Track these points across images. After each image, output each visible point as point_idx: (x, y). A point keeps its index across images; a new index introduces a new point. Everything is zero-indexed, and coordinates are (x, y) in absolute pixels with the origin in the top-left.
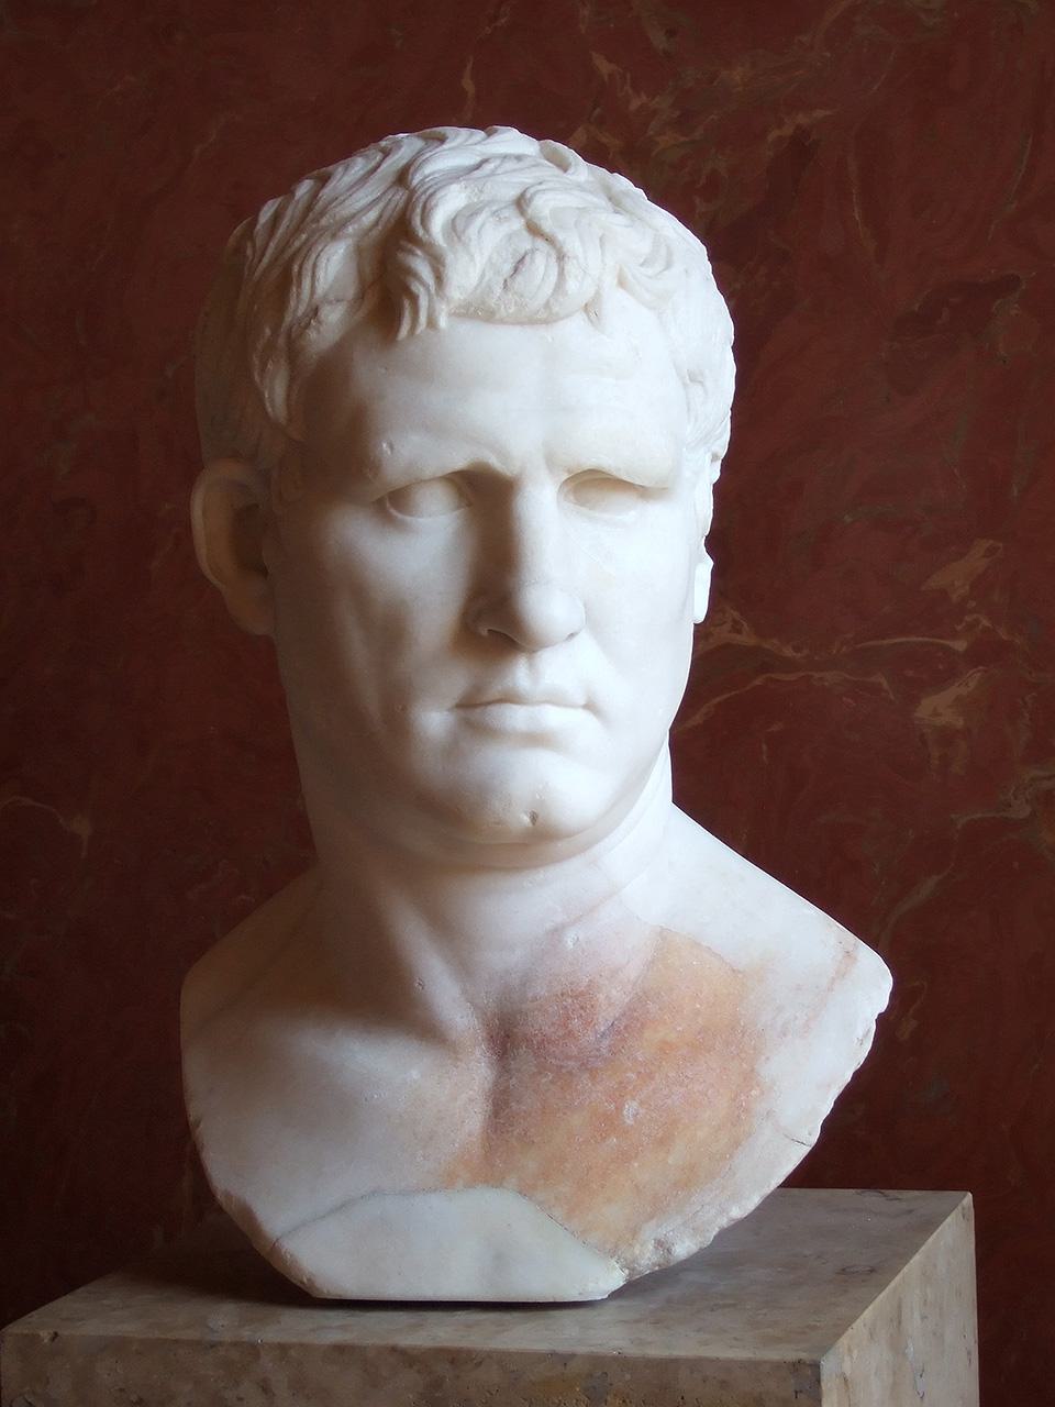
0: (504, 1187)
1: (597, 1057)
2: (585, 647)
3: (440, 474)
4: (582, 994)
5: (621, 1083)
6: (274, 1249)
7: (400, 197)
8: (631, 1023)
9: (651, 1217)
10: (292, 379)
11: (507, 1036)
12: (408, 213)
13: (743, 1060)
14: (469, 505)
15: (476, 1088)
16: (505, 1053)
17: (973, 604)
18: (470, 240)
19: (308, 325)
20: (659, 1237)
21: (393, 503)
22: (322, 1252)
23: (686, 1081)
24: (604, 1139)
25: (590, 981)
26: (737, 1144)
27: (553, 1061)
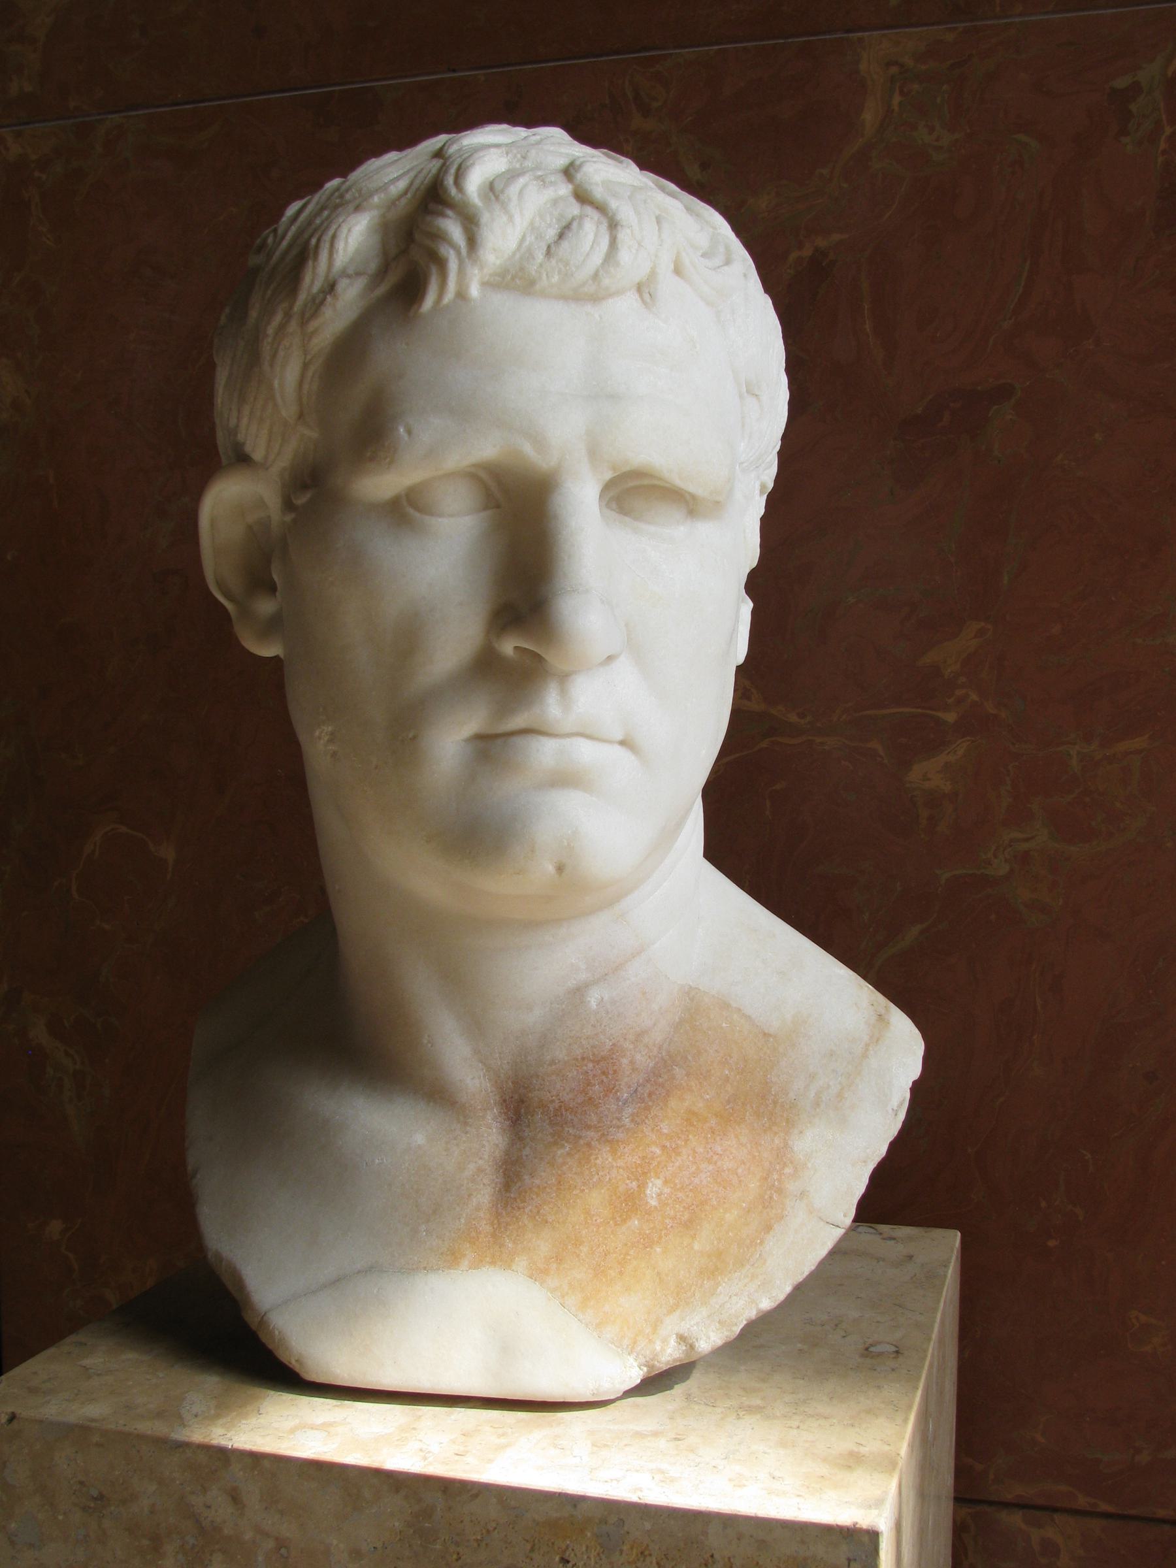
2: (624, 673)
4: (604, 1058)
5: (644, 1158)
6: (263, 1322)
7: (436, 164)
9: (671, 1310)
13: (776, 1133)
15: (486, 1157)
17: (963, 679)
18: (509, 200)
20: (681, 1332)
23: (715, 1158)
24: (624, 1221)
25: (614, 1045)
26: (768, 1228)
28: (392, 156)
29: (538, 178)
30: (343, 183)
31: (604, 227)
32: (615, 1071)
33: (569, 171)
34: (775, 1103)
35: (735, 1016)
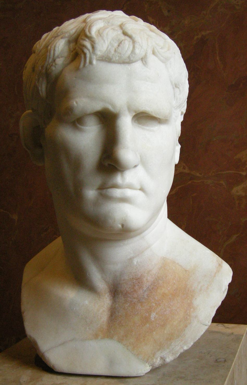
0: (113, 339)
1: (143, 298)
3: (92, 112)
4: (139, 279)
6: (43, 355)
7: (84, 24)
8: (154, 286)
9: (158, 350)
10: (48, 83)
11: (115, 291)
12: (86, 20)
13: (188, 299)
14: (103, 123)
15: (105, 307)
16: (115, 296)
19: (52, 65)
21: (77, 122)
22: (56, 356)
25: (141, 275)
26: (186, 326)
27: (129, 299)
28: (72, 20)
29: (112, 29)
30: (59, 29)
31: (131, 43)
32: (142, 282)
33: (121, 26)
34: (188, 290)
35: (177, 265)
